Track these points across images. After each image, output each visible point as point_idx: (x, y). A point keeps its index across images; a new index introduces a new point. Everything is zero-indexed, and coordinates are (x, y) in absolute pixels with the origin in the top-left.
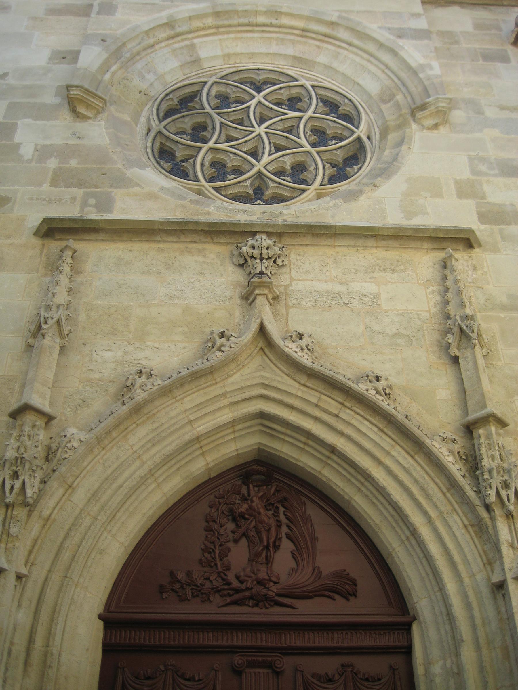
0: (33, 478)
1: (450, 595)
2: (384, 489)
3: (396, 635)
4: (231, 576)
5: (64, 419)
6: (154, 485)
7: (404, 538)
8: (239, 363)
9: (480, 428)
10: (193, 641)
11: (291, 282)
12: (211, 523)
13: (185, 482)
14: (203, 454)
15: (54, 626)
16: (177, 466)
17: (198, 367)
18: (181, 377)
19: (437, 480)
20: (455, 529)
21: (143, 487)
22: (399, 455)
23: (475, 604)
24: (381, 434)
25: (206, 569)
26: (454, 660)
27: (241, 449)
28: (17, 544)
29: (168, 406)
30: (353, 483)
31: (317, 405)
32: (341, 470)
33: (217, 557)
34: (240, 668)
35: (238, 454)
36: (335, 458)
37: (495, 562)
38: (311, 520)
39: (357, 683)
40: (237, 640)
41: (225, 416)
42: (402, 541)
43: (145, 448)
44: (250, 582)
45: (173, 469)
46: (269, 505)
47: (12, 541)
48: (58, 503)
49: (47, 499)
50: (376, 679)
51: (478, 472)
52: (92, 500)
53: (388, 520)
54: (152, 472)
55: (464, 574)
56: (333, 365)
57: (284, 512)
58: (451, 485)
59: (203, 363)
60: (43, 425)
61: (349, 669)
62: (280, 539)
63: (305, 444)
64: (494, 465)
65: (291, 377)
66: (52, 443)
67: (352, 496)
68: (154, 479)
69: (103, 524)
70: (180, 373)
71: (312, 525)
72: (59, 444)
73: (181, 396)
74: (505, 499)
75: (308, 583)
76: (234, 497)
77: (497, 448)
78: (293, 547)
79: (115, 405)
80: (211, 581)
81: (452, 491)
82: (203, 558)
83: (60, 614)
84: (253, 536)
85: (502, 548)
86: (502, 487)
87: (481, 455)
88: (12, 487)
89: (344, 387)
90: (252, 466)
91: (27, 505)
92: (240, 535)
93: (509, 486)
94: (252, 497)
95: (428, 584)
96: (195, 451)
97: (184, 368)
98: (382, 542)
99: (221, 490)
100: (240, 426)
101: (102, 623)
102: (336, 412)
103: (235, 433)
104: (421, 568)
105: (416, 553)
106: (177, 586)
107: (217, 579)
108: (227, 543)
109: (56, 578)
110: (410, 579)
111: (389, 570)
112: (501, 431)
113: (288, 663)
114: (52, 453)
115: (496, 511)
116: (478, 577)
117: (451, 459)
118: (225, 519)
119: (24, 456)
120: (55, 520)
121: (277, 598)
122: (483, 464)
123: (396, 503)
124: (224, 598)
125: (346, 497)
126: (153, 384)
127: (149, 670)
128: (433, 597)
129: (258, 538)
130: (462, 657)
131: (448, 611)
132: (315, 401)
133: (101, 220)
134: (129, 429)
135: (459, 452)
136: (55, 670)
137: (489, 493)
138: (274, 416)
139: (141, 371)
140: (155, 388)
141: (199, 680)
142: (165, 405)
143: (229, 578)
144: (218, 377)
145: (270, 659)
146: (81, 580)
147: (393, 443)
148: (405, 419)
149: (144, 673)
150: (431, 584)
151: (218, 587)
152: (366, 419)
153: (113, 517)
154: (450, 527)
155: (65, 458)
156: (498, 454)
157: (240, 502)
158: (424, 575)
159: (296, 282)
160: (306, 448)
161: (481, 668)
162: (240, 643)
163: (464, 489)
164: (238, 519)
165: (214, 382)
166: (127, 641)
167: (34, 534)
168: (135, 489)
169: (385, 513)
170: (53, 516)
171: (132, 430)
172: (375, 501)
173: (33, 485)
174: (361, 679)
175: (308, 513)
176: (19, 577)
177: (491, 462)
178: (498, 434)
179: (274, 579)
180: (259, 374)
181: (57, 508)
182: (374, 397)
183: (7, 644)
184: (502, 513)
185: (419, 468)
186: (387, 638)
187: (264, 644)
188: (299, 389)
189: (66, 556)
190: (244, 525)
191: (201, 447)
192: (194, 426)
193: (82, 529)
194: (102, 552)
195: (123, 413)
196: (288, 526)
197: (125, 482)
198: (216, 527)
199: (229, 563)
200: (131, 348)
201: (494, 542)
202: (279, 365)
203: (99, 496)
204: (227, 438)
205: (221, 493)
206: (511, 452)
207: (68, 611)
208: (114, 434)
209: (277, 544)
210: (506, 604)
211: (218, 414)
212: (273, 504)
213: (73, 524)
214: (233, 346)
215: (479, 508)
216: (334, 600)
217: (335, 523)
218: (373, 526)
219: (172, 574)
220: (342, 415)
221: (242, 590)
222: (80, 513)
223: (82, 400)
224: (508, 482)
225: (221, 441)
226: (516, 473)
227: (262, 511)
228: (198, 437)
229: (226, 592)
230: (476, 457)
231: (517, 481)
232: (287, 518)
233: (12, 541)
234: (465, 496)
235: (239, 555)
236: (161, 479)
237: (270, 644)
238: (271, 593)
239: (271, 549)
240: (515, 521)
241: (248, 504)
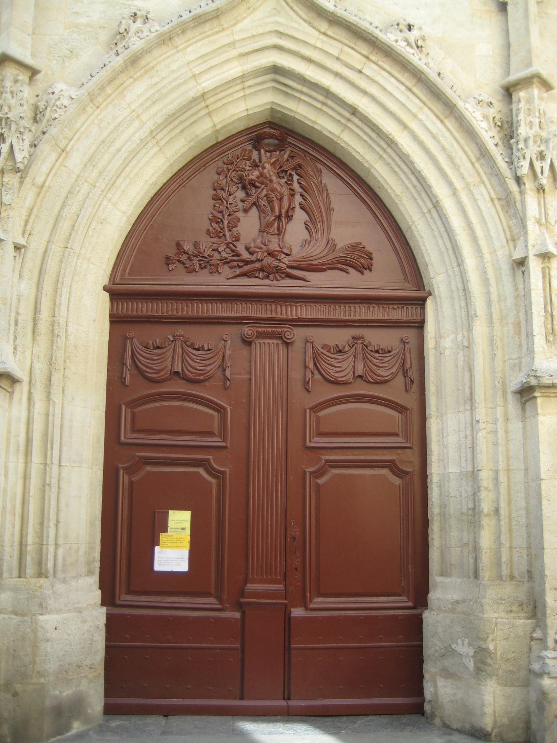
0: (21, 141)
1: (468, 271)
2: (407, 156)
3: (410, 310)
4: (240, 248)
5: (50, 73)
6: (156, 149)
7: (425, 211)
8: (249, 5)
9: (521, 91)
10: (202, 313)
12: (219, 191)
13: (190, 146)
14: (209, 114)
15: (58, 297)
16: (181, 128)
17: (202, 10)
18: (182, 22)
19: (467, 149)
20: (480, 203)
21: (144, 150)
22: (426, 118)
23: (492, 281)
24: (409, 94)
25: (214, 240)
26: (466, 334)
27: (252, 108)
28: (12, 213)
29: (168, 57)
30: (374, 149)
31: (338, 58)
32: (361, 134)
33: (226, 227)
34: (249, 338)
35: (248, 115)
36: (356, 120)
37: (519, 239)
38: (327, 190)
39: (367, 354)
40: (247, 312)
41: (234, 70)
42: (424, 214)
43: (144, 107)
44: (260, 253)
46: (282, 172)
47: (6, 210)
48: (52, 169)
49: (39, 164)
50: (387, 351)
51: (512, 141)
52: (88, 166)
53: (410, 190)
54: (154, 134)
55: (485, 250)
56: (359, 10)
57: (298, 180)
58: (481, 154)
59: (207, 4)
60: (27, 80)
61: (360, 341)
62: (293, 208)
63: (324, 104)
64: (531, 133)
65: (309, 23)
66: (39, 101)
67: (372, 164)
68: (155, 143)
69: (103, 191)
70: (181, 16)
71: (328, 194)
72: (47, 102)
73: (183, 46)
74: (538, 171)
75: (321, 255)
76: (243, 163)
77: (537, 115)
78: (307, 218)
79: (107, 56)
80: (220, 253)
81: (482, 161)
82: (211, 229)
83: (64, 285)
84: (264, 205)
85: (527, 224)
86: (537, 158)
87: (518, 121)
89: (371, 37)
90: (263, 128)
91: (18, 170)
92: (250, 204)
93: (544, 157)
94: (263, 164)
95: (446, 259)
96: (200, 110)
97: (186, 10)
98: (402, 214)
99: (229, 156)
100: (251, 82)
101: (108, 294)
102: (359, 68)
103: (245, 90)
104: (440, 242)
105: (437, 226)
106: (184, 257)
107: (226, 250)
108: (236, 213)
109: (56, 249)
110: (428, 254)
111: (407, 243)
112: (545, 95)
113: (298, 335)
114: (41, 112)
115: (526, 184)
116: (501, 254)
117: (484, 125)
118: (234, 187)
119: (8, 116)
120: (49, 187)
121: (289, 270)
122: (519, 131)
123: (419, 172)
124: (234, 270)
125: (366, 165)
126: (150, 30)
127: (158, 341)
128: (451, 273)
129: (269, 208)
130: (474, 331)
131: (464, 287)
132: (336, 53)
134: (125, 85)
135: (494, 118)
136: (63, 338)
137: (521, 164)
138: (289, 71)
139: (135, 14)
140: (153, 35)
141: (209, 350)
142: (165, 56)
143: (238, 249)
144: (225, 21)
145: (280, 330)
146: (83, 251)
147: (422, 105)
148: (437, 77)
149: (153, 343)
150: (450, 258)
151: (226, 259)
152: (393, 76)
153: (113, 185)
154: (475, 200)
155: (56, 118)
156: (537, 121)
157: (250, 168)
158: (443, 249)
160: (325, 108)
161: (492, 342)
162: (249, 315)
163: (495, 160)
164: (249, 187)
165: (221, 28)
166: (135, 313)
167: (29, 203)
168: (135, 153)
169: (407, 182)
170: (47, 184)
171: (129, 86)
172: (397, 169)
173: (22, 148)
174: (371, 351)
175: (324, 182)
176: (17, 248)
177: (528, 129)
178: (541, 98)
179: (286, 251)
180: (272, 19)
181: (52, 174)
182: (403, 50)
183: (13, 314)
184: (533, 187)
185: (448, 134)
186: (400, 312)
187: (274, 316)
188: (318, 39)
189: (65, 226)
190: (255, 193)
191: (207, 106)
192: (198, 81)
193: (80, 197)
194: (102, 222)
195: (117, 65)
196: (302, 195)
197: (123, 145)
198: (225, 195)
199: (239, 233)
201: (520, 217)
202: (296, 8)
203: (96, 160)
204: (236, 96)
205: (230, 158)
206: (552, 120)
207: (72, 282)
208: (109, 90)
209: (290, 215)
210: (524, 281)
211: (226, 67)
212: (286, 172)
213: (69, 192)
215: (510, 180)
216: (348, 273)
217: (353, 193)
218: (393, 197)
219: (178, 245)
221: (252, 262)
222: (77, 180)
223: (69, 50)
224: (544, 153)
225: (229, 99)
226: (555, 143)
227: (274, 178)
228: (203, 95)
229: (235, 264)
230: (512, 124)
231: (555, 152)
232: (301, 187)
233: (6, 210)
234: (496, 167)
235: (249, 226)
237: (280, 316)
238: (281, 265)
239: (283, 219)
240: (545, 196)
241: (259, 171)
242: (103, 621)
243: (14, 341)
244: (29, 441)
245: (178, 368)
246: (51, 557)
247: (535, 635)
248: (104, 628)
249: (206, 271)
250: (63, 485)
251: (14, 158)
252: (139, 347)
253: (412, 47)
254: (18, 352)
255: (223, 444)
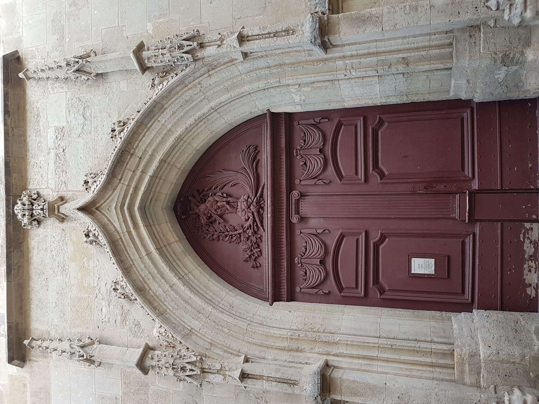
6: (190, 275)
11: (49, 188)
12: (214, 237)
14: (169, 245)
26: (291, 87)
36: (169, 160)
45: (179, 263)
65: (115, 189)
88: (191, 370)
96: (167, 250)
102: (138, 159)
132: (130, 173)
133: (8, 323)
139: (114, 289)
141: (306, 243)
159: (49, 185)
176: (247, 360)
181: (204, 338)
191: (165, 246)
200: (99, 296)
202: (107, 197)
204: (159, 229)
212: (201, 198)
214: (94, 228)
220: (140, 154)
221: (254, 217)
236: (186, 272)
242: (482, 312)
243: (303, 364)
244: (364, 358)
245: (318, 262)
246: (440, 347)
247: (492, 25)
248: (488, 311)
249: (261, 244)
250: (392, 336)
251: (195, 362)
252: (305, 284)
253: (124, 129)
254: (309, 362)
255: (363, 234)
